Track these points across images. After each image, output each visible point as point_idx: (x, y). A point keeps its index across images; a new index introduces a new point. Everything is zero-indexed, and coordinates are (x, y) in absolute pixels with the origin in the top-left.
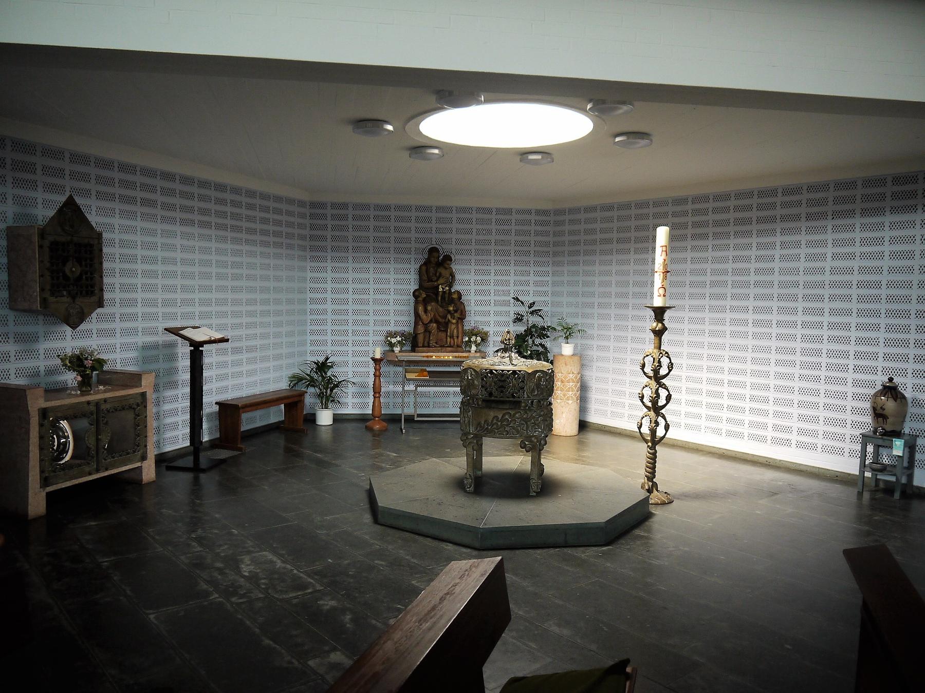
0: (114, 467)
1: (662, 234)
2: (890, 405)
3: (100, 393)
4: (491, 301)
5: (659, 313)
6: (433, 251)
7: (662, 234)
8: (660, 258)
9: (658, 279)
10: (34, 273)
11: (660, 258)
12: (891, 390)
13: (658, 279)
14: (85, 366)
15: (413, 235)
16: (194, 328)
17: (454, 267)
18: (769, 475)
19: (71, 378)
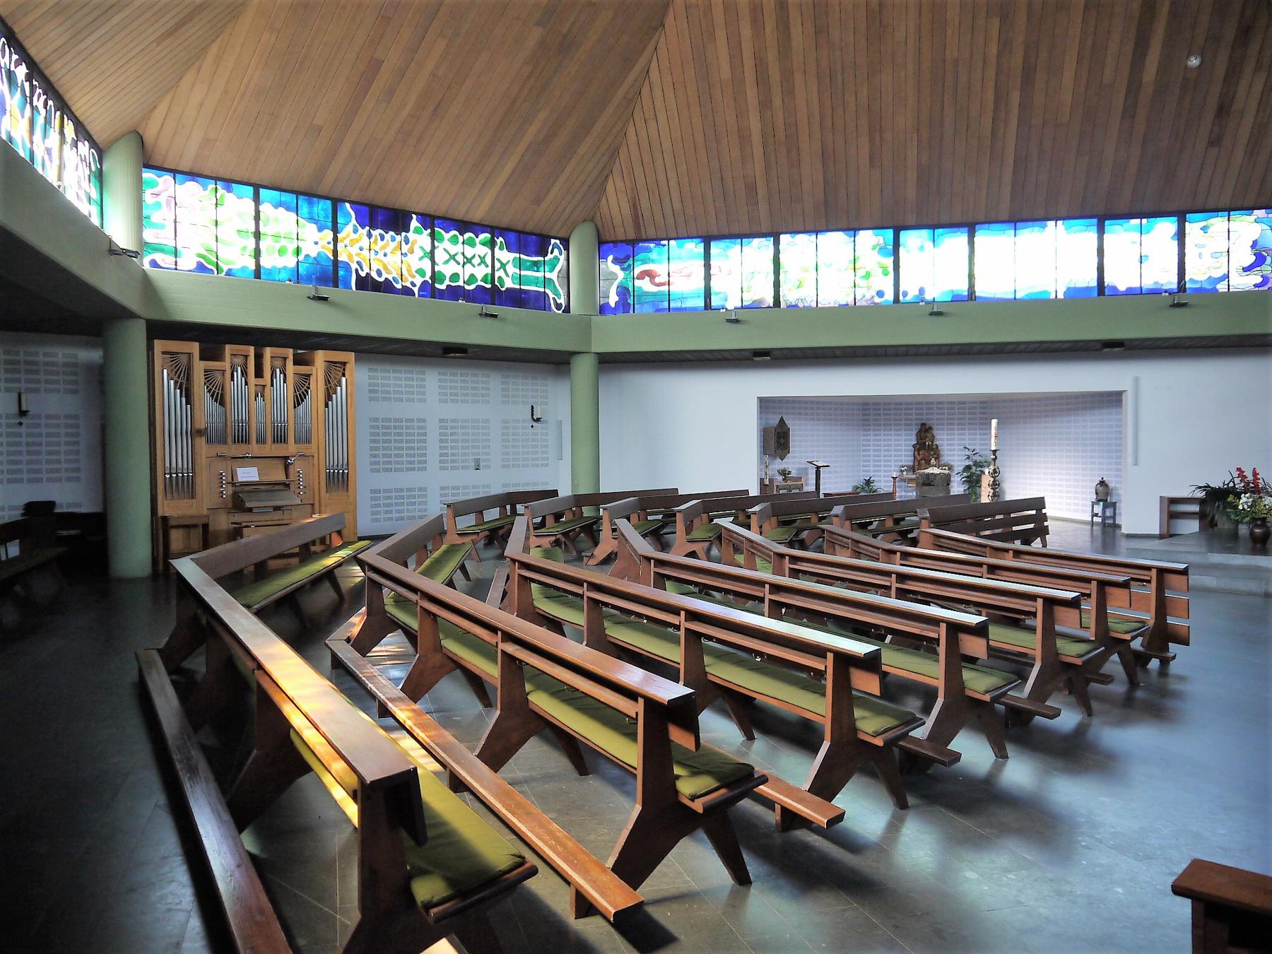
0: (513, 814)
1: (994, 422)
2: (1101, 489)
3: (789, 483)
4: (954, 451)
5: (995, 452)
6: (923, 424)
7: (994, 422)
8: (993, 431)
9: (993, 439)
10: (772, 443)
11: (993, 431)
12: (1102, 483)
13: (993, 439)
14: (784, 473)
15: (914, 417)
16: (505, 593)
17: (935, 432)
18: (1066, 524)
19: (780, 478)
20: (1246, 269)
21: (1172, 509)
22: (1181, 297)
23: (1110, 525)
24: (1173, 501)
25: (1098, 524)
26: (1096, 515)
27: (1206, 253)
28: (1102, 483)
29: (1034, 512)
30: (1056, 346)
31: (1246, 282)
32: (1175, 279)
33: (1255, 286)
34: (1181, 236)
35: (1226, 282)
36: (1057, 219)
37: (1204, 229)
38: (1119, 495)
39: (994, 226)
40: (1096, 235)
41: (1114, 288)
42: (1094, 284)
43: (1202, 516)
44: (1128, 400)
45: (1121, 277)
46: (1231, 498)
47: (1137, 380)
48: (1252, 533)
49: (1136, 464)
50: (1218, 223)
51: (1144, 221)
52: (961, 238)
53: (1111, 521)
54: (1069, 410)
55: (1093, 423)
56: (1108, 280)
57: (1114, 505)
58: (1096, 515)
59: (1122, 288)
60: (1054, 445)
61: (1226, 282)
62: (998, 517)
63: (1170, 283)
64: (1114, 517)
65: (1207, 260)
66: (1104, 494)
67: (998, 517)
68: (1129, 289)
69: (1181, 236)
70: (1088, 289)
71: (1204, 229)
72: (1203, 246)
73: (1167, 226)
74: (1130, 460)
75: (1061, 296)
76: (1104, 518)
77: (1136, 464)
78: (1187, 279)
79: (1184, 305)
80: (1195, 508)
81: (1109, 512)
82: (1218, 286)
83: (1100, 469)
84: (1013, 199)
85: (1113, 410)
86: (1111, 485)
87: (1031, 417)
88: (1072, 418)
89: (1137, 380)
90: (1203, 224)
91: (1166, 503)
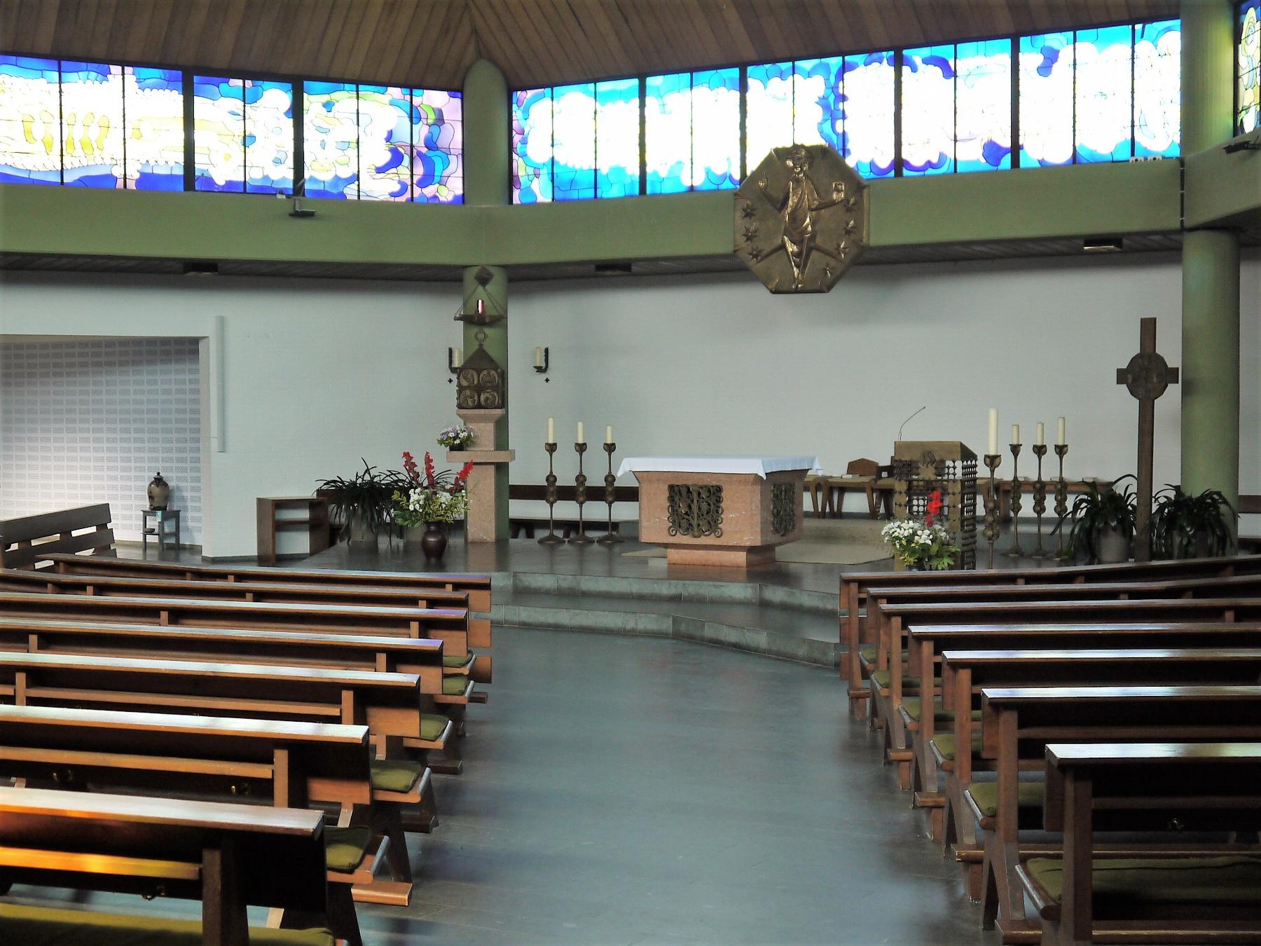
2: (156, 490)
12: (159, 481)
20: (380, 170)
21: (273, 515)
22: (299, 201)
23: (170, 547)
24: (280, 504)
25: (153, 546)
26: (151, 532)
27: (331, 139)
28: (159, 481)
29: (93, 529)
30: (114, 263)
31: (380, 188)
32: (290, 175)
33: (393, 195)
34: (297, 112)
35: (354, 186)
36: (123, 64)
37: (328, 106)
38: (183, 499)
39: (24, 61)
40: (738, 94)
41: (209, 181)
42: (179, 171)
43: (313, 526)
44: (209, 352)
45: (220, 166)
46: (396, 496)
47: (222, 321)
48: (424, 543)
49: (223, 450)
50: (344, 98)
51: (249, 83)
52: (688, 75)
53: (172, 541)
54: (98, 364)
55: (153, 386)
56: (201, 164)
57: (176, 515)
58: (151, 532)
59: (220, 181)
60: (73, 421)
61: (354, 186)
62: (980, 511)
63: (284, 179)
64: (176, 534)
65: (332, 152)
66: (162, 498)
67: (980, 511)
68: (230, 184)
69: (297, 112)
70: (171, 177)
71: (328, 106)
72: (326, 132)
73: (276, 97)
74: (215, 444)
75: (131, 185)
76: (162, 535)
77: (223, 450)
78: (307, 176)
79: (309, 215)
80: (304, 514)
81: (169, 527)
82: (346, 191)
83: (151, 460)
84: (60, 20)
85: (187, 366)
86: (171, 484)
87: (31, 375)
88: (104, 378)
89: (222, 321)
90: (325, 98)
91: (270, 508)
